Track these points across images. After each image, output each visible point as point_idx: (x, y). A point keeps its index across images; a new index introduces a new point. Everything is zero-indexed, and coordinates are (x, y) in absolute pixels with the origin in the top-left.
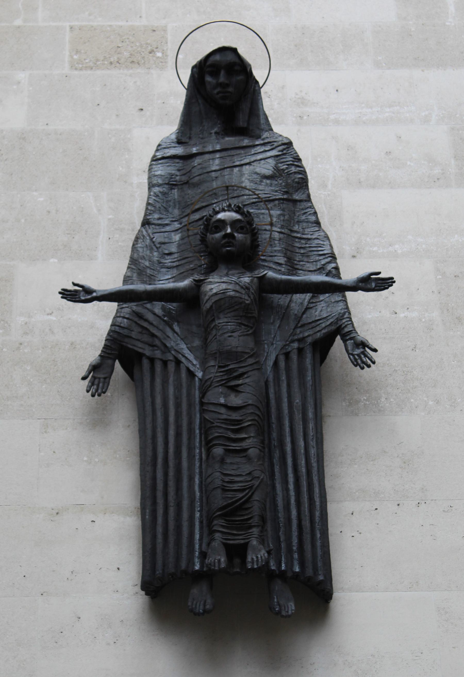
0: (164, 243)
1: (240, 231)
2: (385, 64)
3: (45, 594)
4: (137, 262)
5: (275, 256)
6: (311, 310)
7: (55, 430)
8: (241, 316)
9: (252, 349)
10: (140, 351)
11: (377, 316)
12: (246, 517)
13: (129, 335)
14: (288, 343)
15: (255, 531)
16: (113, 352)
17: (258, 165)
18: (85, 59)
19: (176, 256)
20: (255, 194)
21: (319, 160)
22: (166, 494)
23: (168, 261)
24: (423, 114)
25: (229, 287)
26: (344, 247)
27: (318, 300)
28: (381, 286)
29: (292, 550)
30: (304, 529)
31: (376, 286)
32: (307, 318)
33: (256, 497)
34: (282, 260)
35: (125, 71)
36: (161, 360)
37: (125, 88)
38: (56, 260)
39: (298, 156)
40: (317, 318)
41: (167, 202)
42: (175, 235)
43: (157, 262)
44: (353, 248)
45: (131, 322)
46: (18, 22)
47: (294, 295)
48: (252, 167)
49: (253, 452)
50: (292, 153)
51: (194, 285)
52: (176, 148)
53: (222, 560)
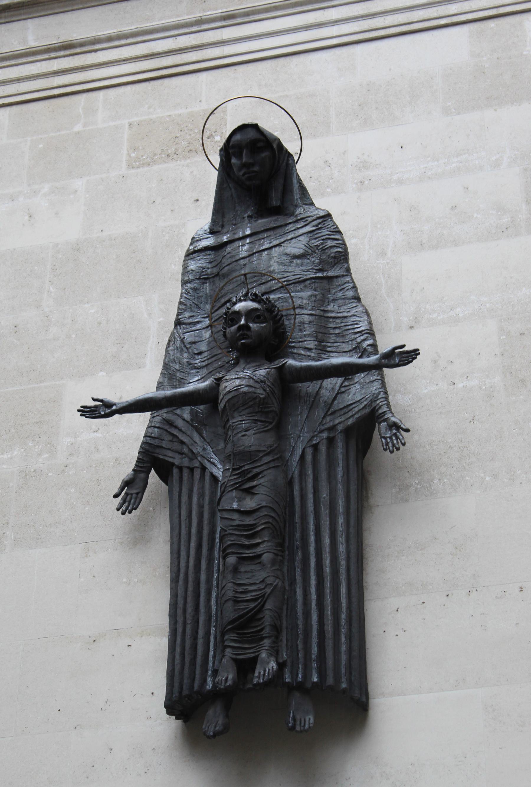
0: (194, 343)
1: (256, 320)
2: (455, 109)
3: (78, 728)
4: (168, 367)
5: (305, 341)
6: (343, 395)
7: (95, 553)
8: (256, 412)
9: (270, 446)
10: (171, 460)
11: (433, 389)
12: (259, 628)
13: (160, 445)
14: (316, 433)
15: (267, 642)
16: (145, 465)
17: (289, 245)
18: (142, 156)
19: (206, 354)
20: (275, 279)
21: (379, 226)
22: (185, 611)
23: (197, 361)
24: (493, 159)
25: (242, 383)
26: (401, 318)
27: (351, 383)
28: (405, 360)
29: (311, 658)
30: (326, 635)
31: (400, 361)
32: (338, 405)
33: (268, 606)
34: (312, 344)
35: (183, 162)
36: (188, 468)
37: (181, 180)
38: (104, 374)
39: (337, 228)
40: (349, 403)
41: (199, 297)
42: (206, 332)
43: (186, 364)
44: (411, 318)
45: (162, 430)
46: (78, 128)
47: (325, 381)
48: (282, 249)
49: (267, 557)
50: (329, 226)
51: (214, 385)
52: (208, 239)
53: (230, 677)
